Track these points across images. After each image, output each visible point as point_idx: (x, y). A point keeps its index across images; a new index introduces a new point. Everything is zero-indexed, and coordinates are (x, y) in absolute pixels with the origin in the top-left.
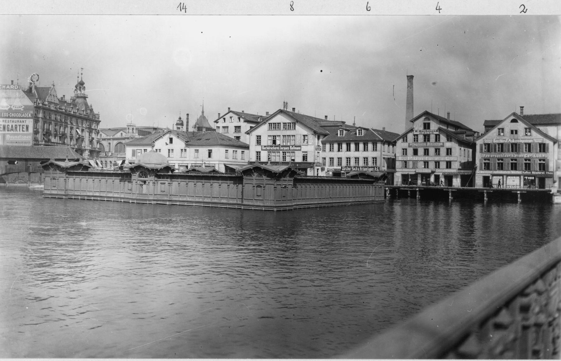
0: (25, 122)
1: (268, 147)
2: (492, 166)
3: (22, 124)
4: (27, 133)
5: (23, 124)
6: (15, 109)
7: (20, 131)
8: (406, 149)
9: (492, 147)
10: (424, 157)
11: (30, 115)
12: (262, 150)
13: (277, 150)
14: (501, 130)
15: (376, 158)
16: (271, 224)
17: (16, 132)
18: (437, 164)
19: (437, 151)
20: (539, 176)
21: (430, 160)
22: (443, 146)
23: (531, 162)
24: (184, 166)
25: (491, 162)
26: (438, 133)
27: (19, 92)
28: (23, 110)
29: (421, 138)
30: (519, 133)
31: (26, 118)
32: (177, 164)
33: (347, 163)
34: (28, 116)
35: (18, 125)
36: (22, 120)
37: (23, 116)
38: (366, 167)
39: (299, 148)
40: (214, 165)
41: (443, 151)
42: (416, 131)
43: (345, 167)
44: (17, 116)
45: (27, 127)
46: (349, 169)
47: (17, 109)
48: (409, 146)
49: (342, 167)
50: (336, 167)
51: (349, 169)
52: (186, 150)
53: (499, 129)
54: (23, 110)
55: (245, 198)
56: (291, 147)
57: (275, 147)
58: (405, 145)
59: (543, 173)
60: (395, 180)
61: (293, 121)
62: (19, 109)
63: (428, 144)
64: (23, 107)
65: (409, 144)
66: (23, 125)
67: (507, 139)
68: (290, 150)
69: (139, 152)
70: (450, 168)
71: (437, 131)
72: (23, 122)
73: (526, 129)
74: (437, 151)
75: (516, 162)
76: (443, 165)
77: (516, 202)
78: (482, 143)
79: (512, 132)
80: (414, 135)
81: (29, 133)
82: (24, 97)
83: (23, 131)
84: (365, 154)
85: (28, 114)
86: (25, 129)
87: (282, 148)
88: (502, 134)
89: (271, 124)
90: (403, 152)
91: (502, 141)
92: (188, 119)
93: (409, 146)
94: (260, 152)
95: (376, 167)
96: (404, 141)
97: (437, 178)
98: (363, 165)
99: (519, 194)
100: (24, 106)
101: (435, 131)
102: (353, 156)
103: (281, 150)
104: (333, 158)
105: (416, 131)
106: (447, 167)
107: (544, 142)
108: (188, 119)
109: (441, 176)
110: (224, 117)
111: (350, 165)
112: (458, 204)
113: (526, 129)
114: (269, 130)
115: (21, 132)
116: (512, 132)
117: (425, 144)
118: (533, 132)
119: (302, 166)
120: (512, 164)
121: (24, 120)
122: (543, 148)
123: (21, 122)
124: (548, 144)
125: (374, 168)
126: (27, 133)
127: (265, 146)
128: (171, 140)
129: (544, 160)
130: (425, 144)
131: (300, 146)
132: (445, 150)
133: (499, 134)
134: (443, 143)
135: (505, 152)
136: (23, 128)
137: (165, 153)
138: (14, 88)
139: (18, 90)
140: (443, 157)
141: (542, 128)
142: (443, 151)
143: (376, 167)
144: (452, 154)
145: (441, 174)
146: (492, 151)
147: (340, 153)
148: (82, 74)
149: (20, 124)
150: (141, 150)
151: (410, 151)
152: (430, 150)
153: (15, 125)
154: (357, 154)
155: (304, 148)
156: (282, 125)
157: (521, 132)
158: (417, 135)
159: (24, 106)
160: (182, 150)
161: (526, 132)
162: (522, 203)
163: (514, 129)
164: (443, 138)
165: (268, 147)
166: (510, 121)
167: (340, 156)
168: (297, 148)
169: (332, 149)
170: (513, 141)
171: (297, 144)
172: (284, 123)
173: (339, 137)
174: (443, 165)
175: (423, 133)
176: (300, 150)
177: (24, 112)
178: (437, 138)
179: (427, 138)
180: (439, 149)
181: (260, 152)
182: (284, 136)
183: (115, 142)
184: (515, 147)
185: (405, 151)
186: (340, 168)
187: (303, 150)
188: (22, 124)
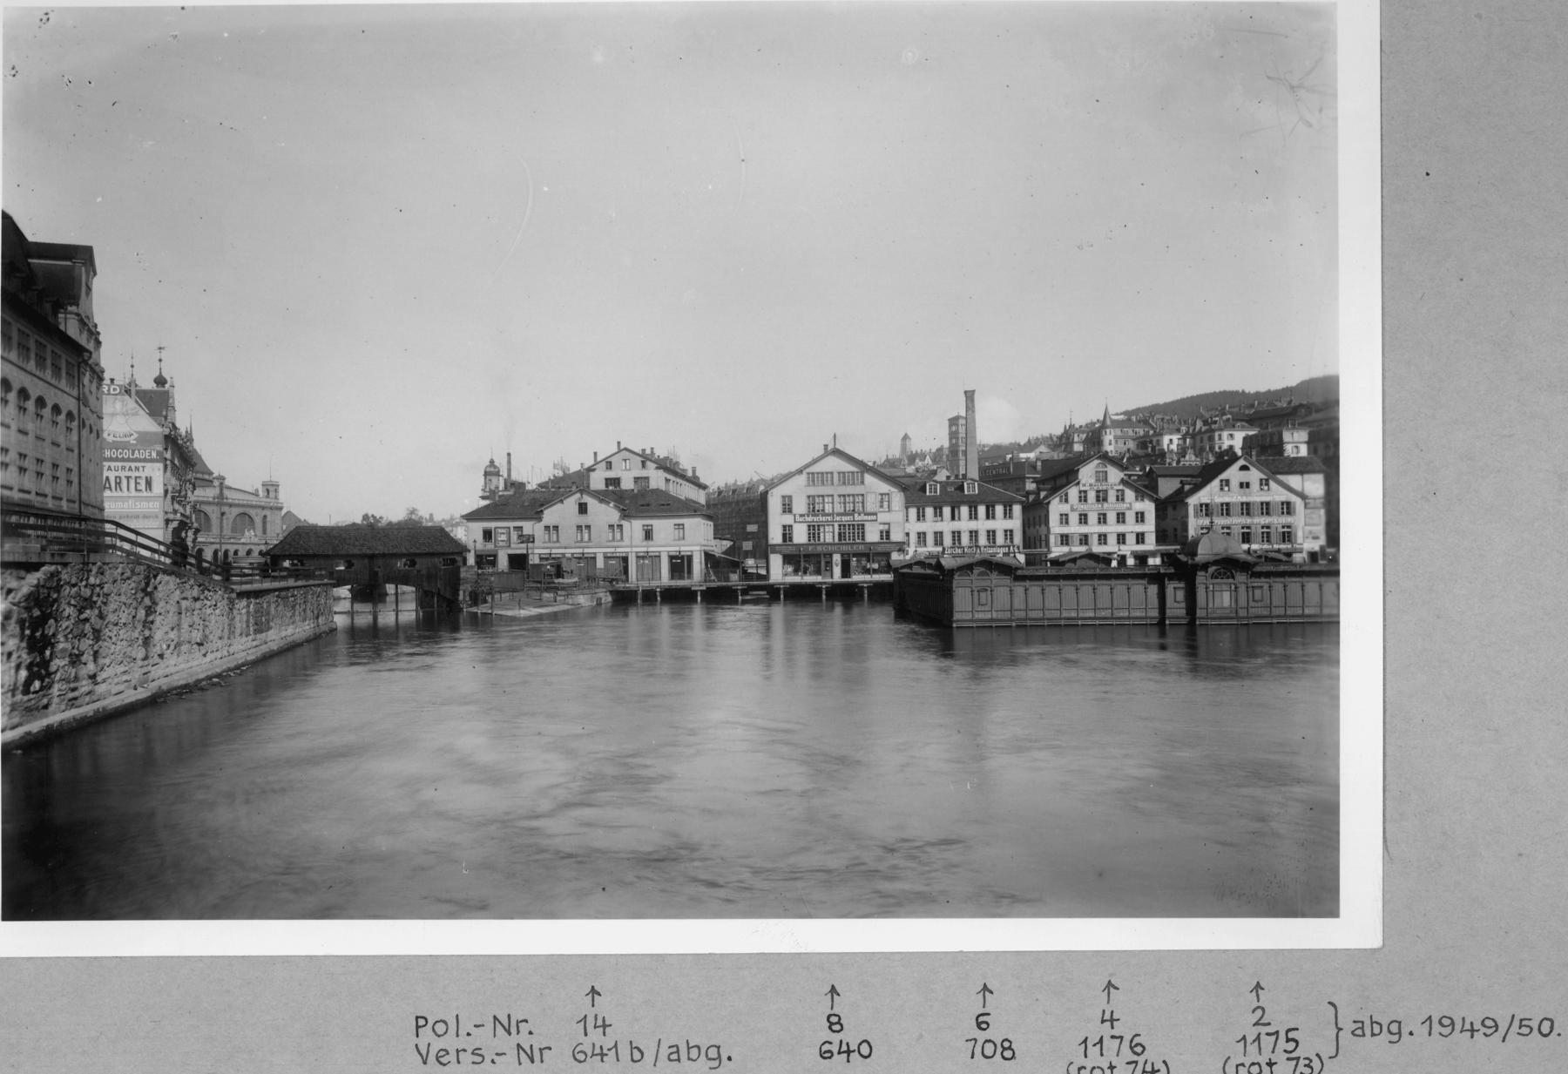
0: (141, 469)
1: (808, 516)
2: (1273, 538)
3: (134, 474)
4: (149, 494)
5: (137, 474)
6: (115, 439)
7: (128, 489)
8: (1067, 515)
10: (1100, 527)
11: (154, 455)
12: (795, 522)
13: (828, 521)
14: (1224, 483)
15: (1011, 531)
17: (119, 494)
18: (1121, 538)
19: (1121, 518)
21: (1109, 531)
22: (1130, 509)
23: (1253, 530)
24: (617, 557)
25: (1272, 530)
26: (1121, 487)
27: (123, 401)
28: (135, 442)
29: (1092, 496)
30: (1251, 486)
31: (145, 460)
32: (666, 553)
33: (954, 540)
34: (150, 455)
35: (123, 478)
36: (133, 465)
37: (136, 455)
38: (993, 547)
39: (874, 517)
40: (657, 554)
41: (1130, 517)
42: (1084, 485)
43: (951, 547)
44: (120, 457)
45: (149, 483)
46: (960, 551)
47: (118, 439)
48: (1073, 510)
49: (944, 549)
50: (931, 548)
51: (960, 551)
52: (621, 526)
53: (1221, 481)
54: (135, 442)
55: (1101, 606)
57: (822, 516)
58: (1065, 508)
59: (1289, 546)
60: (598, 564)
61: (1265, 477)
62: (127, 439)
63: (1106, 505)
64: (136, 436)
66: (136, 477)
67: (1235, 497)
69: (503, 533)
70: (1143, 542)
71: (1119, 484)
72: (137, 469)
73: (1261, 480)
74: (1121, 518)
75: (1268, 530)
76: (1131, 539)
77: (820, 599)
78: (1197, 502)
79: (1241, 485)
80: (1080, 492)
81: (152, 495)
82: (136, 414)
83: (136, 490)
84: (990, 525)
85: (150, 453)
86: (143, 486)
87: (838, 518)
88: (1226, 488)
89: (813, 473)
90: (1061, 519)
91: (1227, 500)
92: (509, 462)
93: (1073, 510)
94: (791, 526)
95: (1014, 547)
96: (1061, 501)
97: (1123, 559)
98: (987, 544)
100: (136, 432)
101: (1115, 485)
102: (965, 529)
103: (836, 521)
104: (924, 534)
105: (1084, 485)
106: (1138, 543)
107: (1288, 500)
108: (509, 462)
109: (1128, 556)
110: (609, 460)
111: (960, 543)
112: (839, 601)
113: (1261, 480)
114: (809, 485)
115: (133, 493)
116: (1241, 485)
117: (1100, 506)
118: (1272, 483)
119: (880, 549)
120: (1243, 533)
121: (139, 464)
122: (1288, 508)
123: (130, 469)
124: (1295, 503)
125: (1009, 547)
126: (149, 494)
127: (801, 516)
128: (583, 508)
129: (1289, 527)
130: (1100, 506)
131: (875, 514)
134: (1130, 504)
136: (136, 483)
137: (568, 534)
138: (109, 390)
139: (119, 397)
140: (1131, 527)
141: (1280, 477)
142: (1130, 517)
143: (1014, 547)
144: (1146, 520)
145: (1128, 554)
148: (160, 360)
149: (129, 474)
150: (509, 528)
151: (1074, 518)
152: (1108, 516)
153: (116, 477)
154: (973, 525)
155: (882, 517)
156: (836, 476)
157: (1255, 486)
158: (1085, 492)
159: (136, 432)
160: (611, 526)
161: (1261, 484)
162: (702, 601)
163: (1245, 480)
164: (1130, 494)
165: (808, 516)
166: (1238, 468)
168: (870, 518)
169: (1140, 519)
170: (1244, 499)
172: (839, 473)
173: (929, 496)
174: (1131, 539)
175: (1096, 488)
176: (876, 520)
177: (139, 447)
178: (1120, 498)
179: (1102, 497)
180: (1124, 514)
181: (791, 526)
182: (840, 496)
183: (235, 511)
184: (1246, 508)
185: (1064, 519)
186: (940, 549)
187: (879, 520)
188: (134, 474)
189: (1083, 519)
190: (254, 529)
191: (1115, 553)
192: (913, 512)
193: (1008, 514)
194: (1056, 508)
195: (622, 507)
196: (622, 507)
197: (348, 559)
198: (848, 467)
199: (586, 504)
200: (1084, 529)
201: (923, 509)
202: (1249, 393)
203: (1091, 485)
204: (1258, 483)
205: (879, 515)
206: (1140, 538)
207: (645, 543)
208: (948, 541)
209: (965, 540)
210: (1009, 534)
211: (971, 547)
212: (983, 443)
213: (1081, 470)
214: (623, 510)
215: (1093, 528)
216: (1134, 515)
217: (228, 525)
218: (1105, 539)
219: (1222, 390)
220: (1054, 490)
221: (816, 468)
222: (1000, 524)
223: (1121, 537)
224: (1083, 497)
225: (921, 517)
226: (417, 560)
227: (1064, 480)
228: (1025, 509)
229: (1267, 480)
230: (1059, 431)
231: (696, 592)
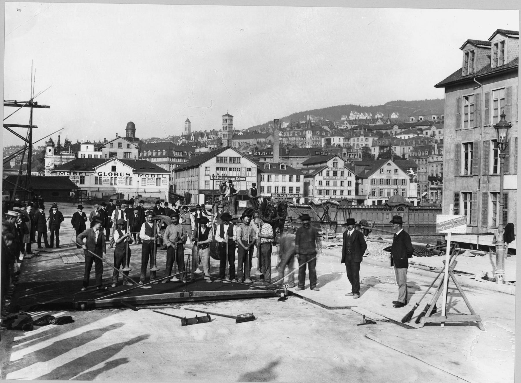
9: (379, 183)
16: (112, 247)
20: (206, 192)
29: (331, 173)
39: (244, 179)
46: (278, 196)
48: (324, 179)
49: (272, 194)
51: (278, 196)
56: (237, 178)
65: (324, 177)
68: (236, 180)
76: (338, 193)
93: (324, 179)
96: (319, 175)
99: (26, 209)
125: (298, 195)
131: (245, 177)
132: (347, 183)
133: (381, 173)
135: (399, 185)
146: (377, 184)
147: (270, 183)
151: (324, 183)
158: (329, 171)
167: (284, 186)
168: (242, 179)
171: (243, 175)
174: (338, 193)
179: (335, 174)
185: (320, 183)
187: (247, 180)
189: (328, 183)
190: (281, 145)
200: (328, 188)
201: (299, 176)
202: (430, 100)
203: (331, 168)
204: (394, 171)
205: (246, 178)
206: (349, 193)
208: (273, 191)
209: (280, 191)
210: (298, 188)
211: (283, 194)
212: (236, 129)
215: (331, 188)
216: (347, 182)
218: (329, 193)
219: (300, 111)
222: (294, 184)
224: (328, 174)
230: (69, 141)
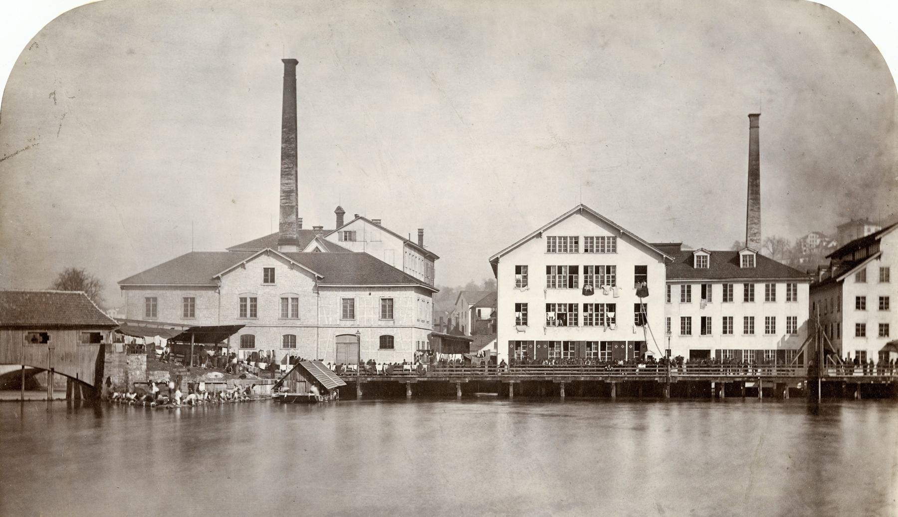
61: (613, 235)
89: (554, 238)
173: (744, 269)
185: (861, 303)
191: (232, 330)
192: (676, 290)
193: (792, 296)
194: (850, 288)
195: (317, 275)
196: (317, 275)
197: (43, 331)
198: (606, 233)
199: (273, 270)
207: (383, 323)
210: (791, 321)
213: (882, 240)
214: (319, 278)
217: (148, 294)
220: (849, 266)
221: (557, 232)
223: (152, 303)
225: (686, 297)
226: (49, 333)
227: (863, 253)
228: (813, 289)
229: (614, 238)
231: (559, 384)
